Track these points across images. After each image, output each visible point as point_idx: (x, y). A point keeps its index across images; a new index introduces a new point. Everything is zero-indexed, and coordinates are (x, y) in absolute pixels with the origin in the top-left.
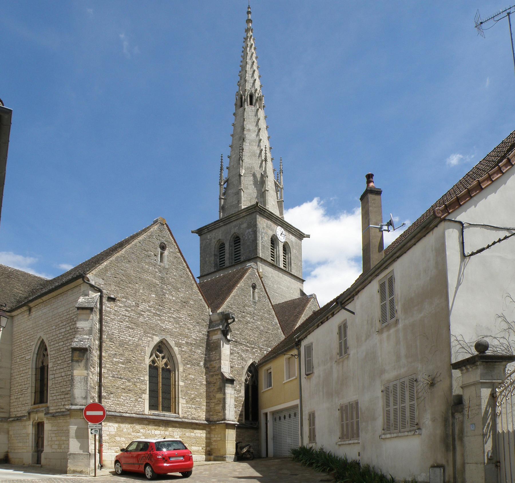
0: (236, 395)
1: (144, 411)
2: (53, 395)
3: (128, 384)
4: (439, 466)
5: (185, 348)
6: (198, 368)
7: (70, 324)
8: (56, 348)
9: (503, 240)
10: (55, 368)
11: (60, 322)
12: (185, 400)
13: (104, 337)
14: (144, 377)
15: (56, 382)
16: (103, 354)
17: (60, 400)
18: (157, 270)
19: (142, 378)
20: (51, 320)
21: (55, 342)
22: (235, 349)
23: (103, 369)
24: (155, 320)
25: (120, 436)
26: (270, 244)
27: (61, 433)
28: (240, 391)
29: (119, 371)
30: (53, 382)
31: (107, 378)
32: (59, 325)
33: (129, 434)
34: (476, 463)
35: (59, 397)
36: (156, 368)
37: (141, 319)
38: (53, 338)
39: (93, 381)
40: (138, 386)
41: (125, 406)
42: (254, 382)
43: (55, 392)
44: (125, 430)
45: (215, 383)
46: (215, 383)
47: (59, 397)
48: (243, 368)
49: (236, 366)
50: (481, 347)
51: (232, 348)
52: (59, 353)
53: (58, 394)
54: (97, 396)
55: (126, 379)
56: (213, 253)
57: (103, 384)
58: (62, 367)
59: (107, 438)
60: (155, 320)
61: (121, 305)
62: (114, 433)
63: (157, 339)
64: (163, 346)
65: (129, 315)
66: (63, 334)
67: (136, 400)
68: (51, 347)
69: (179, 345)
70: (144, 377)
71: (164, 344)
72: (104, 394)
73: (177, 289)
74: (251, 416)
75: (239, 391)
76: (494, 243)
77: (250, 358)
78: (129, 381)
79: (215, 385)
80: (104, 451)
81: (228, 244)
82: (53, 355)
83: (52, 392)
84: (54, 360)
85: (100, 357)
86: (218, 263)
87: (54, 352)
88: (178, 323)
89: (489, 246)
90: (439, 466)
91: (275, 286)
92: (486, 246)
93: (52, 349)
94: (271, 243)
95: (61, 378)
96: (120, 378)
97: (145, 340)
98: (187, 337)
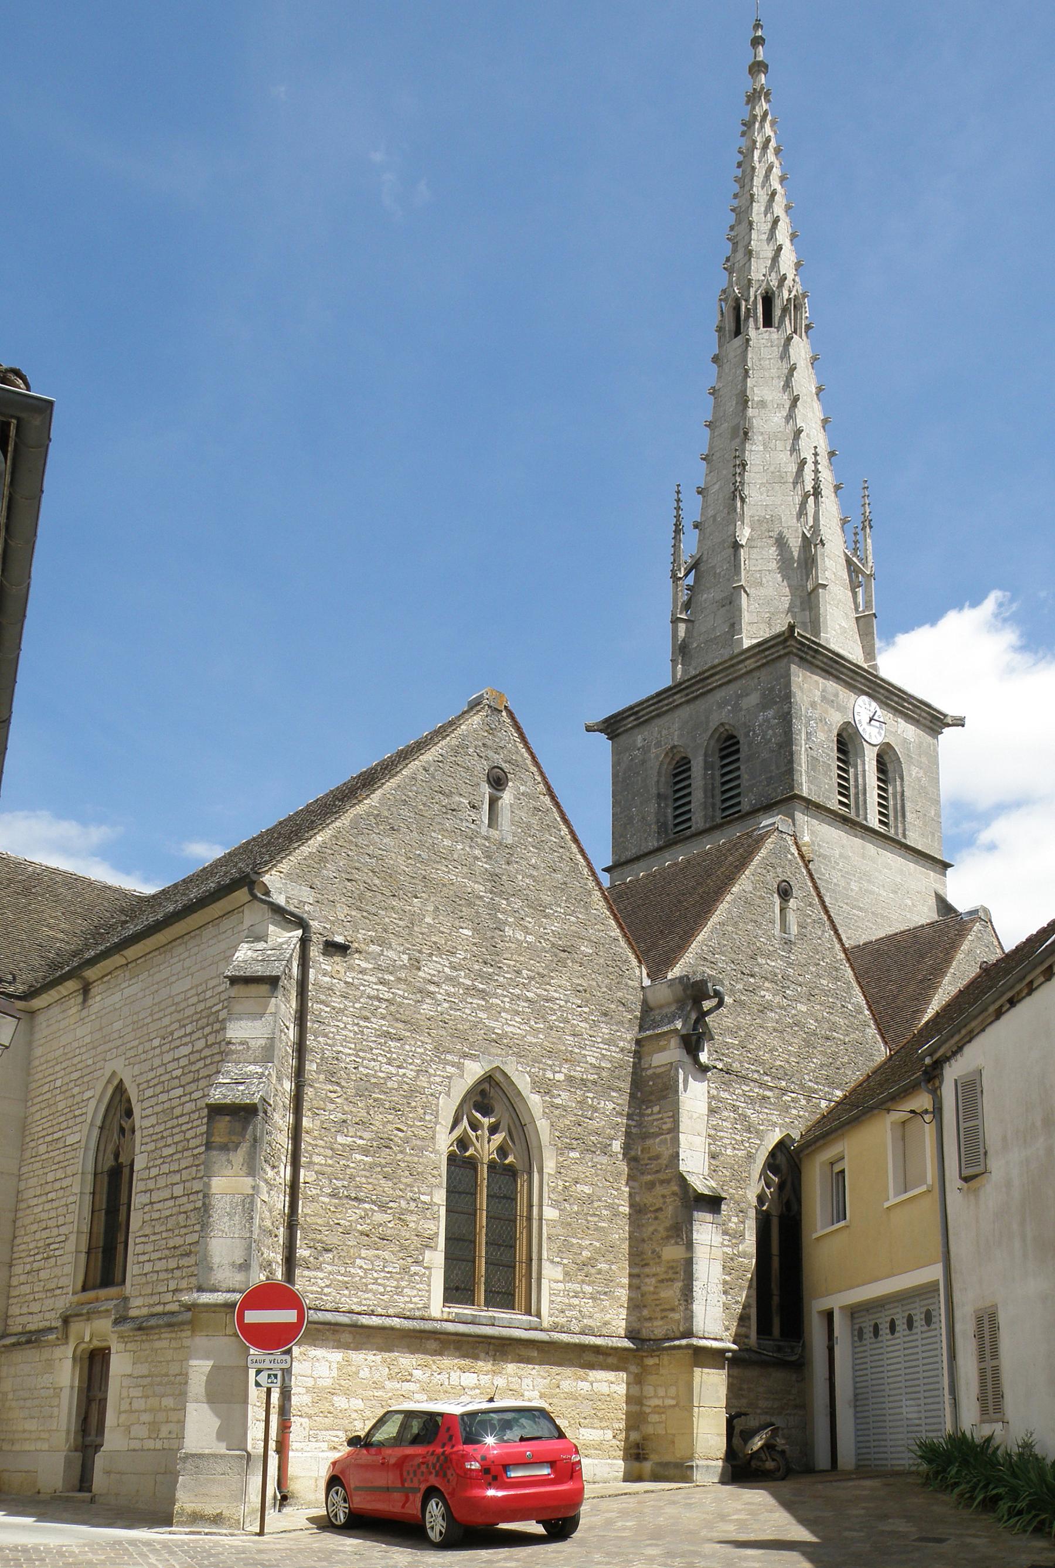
1: (427, 1307)
2: (142, 1258)
3: (379, 1217)
5: (563, 1098)
6: (604, 1159)
10: (154, 1172)
12: (560, 1269)
13: (311, 1067)
14: (431, 1194)
15: (156, 1216)
16: (306, 1123)
17: (163, 1276)
18: (477, 852)
20: (149, 1020)
21: (159, 1089)
23: (302, 1172)
24: (471, 1009)
25: (348, 1393)
26: (835, 754)
28: (742, 1235)
29: (352, 1178)
31: (314, 1199)
33: (378, 1386)
35: (160, 1265)
36: (471, 1164)
38: (152, 1075)
39: (270, 1211)
42: (788, 1205)
44: (364, 1373)
46: (661, 1209)
47: (160, 1265)
48: (750, 1157)
49: (729, 1152)
51: (714, 1092)
53: (158, 1255)
55: (374, 1203)
57: (301, 1220)
58: (175, 1167)
59: (307, 1399)
60: (471, 1009)
63: (475, 1070)
65: (387, 996)
66: (183, 1062)
68: (146, 1104)
69: (544, 1087)
73: (540, 909)
78: (383, 1207)
79: (660, 1215)
83: (139, 1249)
84: (152, 1146)
86: (671, 822)
87: (153, 1120)
91: (854, 886)
93: (149, 1111)
94: (839, 750)
95: (171, 1203)
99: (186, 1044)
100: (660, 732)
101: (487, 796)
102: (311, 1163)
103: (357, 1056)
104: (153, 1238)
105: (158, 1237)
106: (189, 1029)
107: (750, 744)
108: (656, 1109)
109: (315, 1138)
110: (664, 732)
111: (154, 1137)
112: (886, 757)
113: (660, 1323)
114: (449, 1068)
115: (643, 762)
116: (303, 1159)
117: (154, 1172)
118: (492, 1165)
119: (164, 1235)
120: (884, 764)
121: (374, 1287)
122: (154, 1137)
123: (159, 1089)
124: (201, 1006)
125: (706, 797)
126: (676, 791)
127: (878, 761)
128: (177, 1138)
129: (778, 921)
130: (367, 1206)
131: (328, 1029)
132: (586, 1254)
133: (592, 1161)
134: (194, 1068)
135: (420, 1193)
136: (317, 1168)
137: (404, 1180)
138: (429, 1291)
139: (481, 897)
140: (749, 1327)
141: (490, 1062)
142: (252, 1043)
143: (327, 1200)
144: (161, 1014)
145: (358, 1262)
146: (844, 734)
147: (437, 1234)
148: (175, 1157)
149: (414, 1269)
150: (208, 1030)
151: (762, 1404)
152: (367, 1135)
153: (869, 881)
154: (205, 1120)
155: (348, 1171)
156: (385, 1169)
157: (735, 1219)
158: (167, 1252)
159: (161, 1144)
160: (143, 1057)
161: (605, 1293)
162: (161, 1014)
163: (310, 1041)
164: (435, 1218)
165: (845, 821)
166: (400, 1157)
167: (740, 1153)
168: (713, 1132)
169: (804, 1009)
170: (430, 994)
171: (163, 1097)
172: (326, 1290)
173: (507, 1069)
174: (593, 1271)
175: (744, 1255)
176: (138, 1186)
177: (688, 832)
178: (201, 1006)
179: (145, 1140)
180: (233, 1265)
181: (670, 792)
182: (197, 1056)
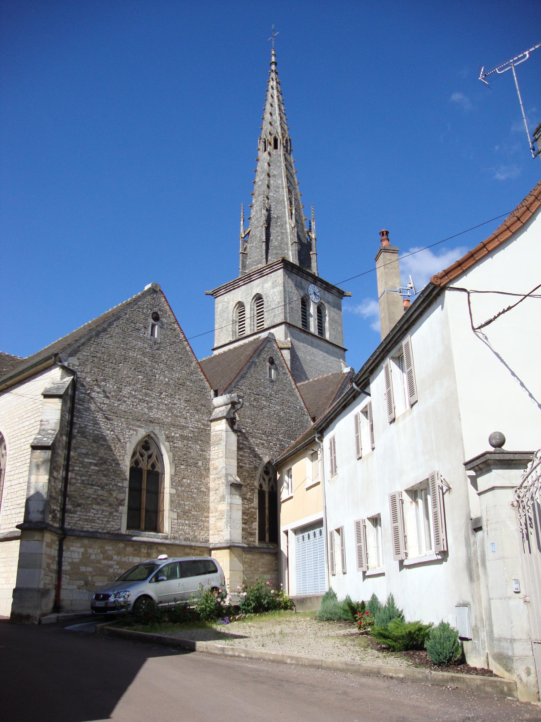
0: (247, 506)
1: (119, 529)
2: (7, 508)
3: (100, 492)
4: (465, 605)
5: (179, 444)
6: (195, 469)
7: (36, 415)
8: (16, 447)
9: (507, 311)
10: (13, 473)
11: (24, 413)
12: (176, 514)
13: (75, 431)
14: (122, 483)
15: (12, 491)
16: (72, 454)
17: (14, 516)
18: (146, 346)
19: (120, 484)
20: (14, 411)
21: (17, 439)
22: (245, 442)
23: (70, 474)
24: (142, 408)
25: (86, 565)
26: (300, 306)
27: (11, 561)
28: (253, 499)
29: (90, 476)
30: (9, 492)
31: (74, 484)
32: (23, 416)
33: (99, 562)
34: (501, 599)
35: (13, 511)
36: (140, 471)
37: (123, 407)
38: (14, 433)
39: (55, 489)
40: (114, 496)
41: (95, 523)
42: (272, 488)
43: (9, 504)
44: (93, 557)
45: (217, 489)
46: (217, 489)
47: (13, 511)
48: (256, 468)
49: (247, 466)
50: (498, 442)
51: (241, 441)
52: (20, 453)
53: (13, 507)
54: (59, 509)
55: (98, 486)
56: (231, 319)
57: (69, 493)
58: (21, 471)
59: (68, 568)
60: (142, 408)
61: (99, 390)
62: (77, 560)
63: (142, 433)
64: (150, 441)
65: (108, 402)
66: (26, 428)
67: (111, 513)
68: (12, 445)
69: (168, 438)
70: (122, 483)
71: (152, 438)
72: (69, 507)
73: (171, 368)
74: (267, 535)
75: (251, 500)
76: (499, 315)
77: (266, 455)
78: (103, 488)
79: (217, 492)
80: (63, 587)
81: (249, 307)
82: (13, 456)
83: (6, 505)
84: (12, 462)
85: (68, 458)
86: (238, 331)
87: (13, 451)
88: (169, 410)
89: (495, 318)
90: (465, 605)
91: (308, 358)
92: (492, 318)
93: (12, 448)
94: (302, 304)
95: (18, 486)
96: (91, 485)
97: (127, 434)
98: (183, 428)
99: (27, 421)
100: (234, 296)
101: (151, 324)
102: (74, 470)
103: (94, 427)
104: (11, 500)
105: (12, 500)
106: (29, 415)
107: (268, 301)
108: (216, 448)
109: (76, 460)
110: (235, 296)
111: (14, 458)
112: (321, 308)
113: (217, 536)
114: (131, 432)
115: (227, 307)
116: (70, 468)
117: (13, 473)
118: (149, 472)
119: (16, 499)
120: (320, 310)
121: (98, 521)
122: (14, 458)
123: (17, 439)
124: (34, 406)
125: (251, 321)
126: (240, 319)
127: (318, 309)
128: (22, 459)
129: (268, 373)
130: (96, 487)
131: (83, 416)
132: (187, 507)
133: (190, 469)
134: (30, 430)
135: (118, 482)
136: (76, 472)
137: (112, 477)
138: (121, 523)
139: (147, 363)
140: (255, 538)
141: (148, 429)
142: (51, 422)
143: (79, 485)
144: (19, 408)
145: (92, 510)
146: (304, 299)
147: (124, 499)
148: (21, 467)
149: (115, 514)
150: (36, 415)
151: (261, 570)
152: (97, 458)
153: (314, 356)
154: (30, 453)
155: (89, 473)
156: (104, 472)
157: (249, 494)
158: (16, 506)
159: (16, 461)
160: (11, 426)
161: (195, 524)
162: (19, 408)
163: (75, 420)
164: (124, 492)
165: (304, 332)
166: (110, 467)
167: (251, 466)
168: (240, 458)
169: (279, 408)
170: (125, 402)
171: (18, 442)
172: (78, 522)
173: (156, 432)
174: (190, 515)
175: (253, 508)
176: (6, 478)
177: (244, 335)
178: (34, 406)
179: (11, 460)
180: (38, 511)
181: (237, 319)
182: (31, 426)
